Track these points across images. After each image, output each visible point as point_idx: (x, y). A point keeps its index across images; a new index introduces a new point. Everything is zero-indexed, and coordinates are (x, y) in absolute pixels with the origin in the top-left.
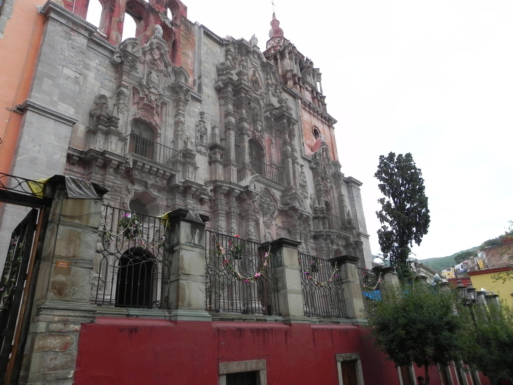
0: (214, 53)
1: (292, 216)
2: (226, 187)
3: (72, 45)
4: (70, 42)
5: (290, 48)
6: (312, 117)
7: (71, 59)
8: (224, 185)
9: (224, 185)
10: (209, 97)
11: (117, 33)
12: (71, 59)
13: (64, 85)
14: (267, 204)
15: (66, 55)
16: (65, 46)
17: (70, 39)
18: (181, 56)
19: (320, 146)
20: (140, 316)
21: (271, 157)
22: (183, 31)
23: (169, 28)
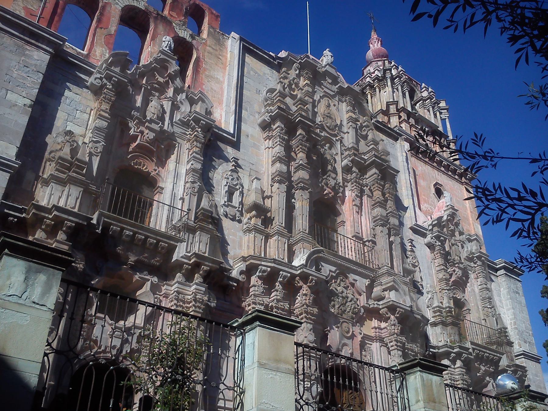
0: (259, 75)
1: (389, 318)
2: (266, 266)
3: (26, 62)
4: (23, 58)
5: (485, 218)
6: (436, 172)
7: (21, 81)
8: (263, 263)
9: (263, 263)
10: (248, 136)
11: (104, 49)
12: (21, 81)
13: (6, 116)
14: (342, 297)
15: (15, 75)
16: (14, 63)
17: (24, 55)
18: (205, 81)
19: (445, 211)
20: (339, 391)
21: (29, 50)
22: (210, 46)
23: (188, 42)
